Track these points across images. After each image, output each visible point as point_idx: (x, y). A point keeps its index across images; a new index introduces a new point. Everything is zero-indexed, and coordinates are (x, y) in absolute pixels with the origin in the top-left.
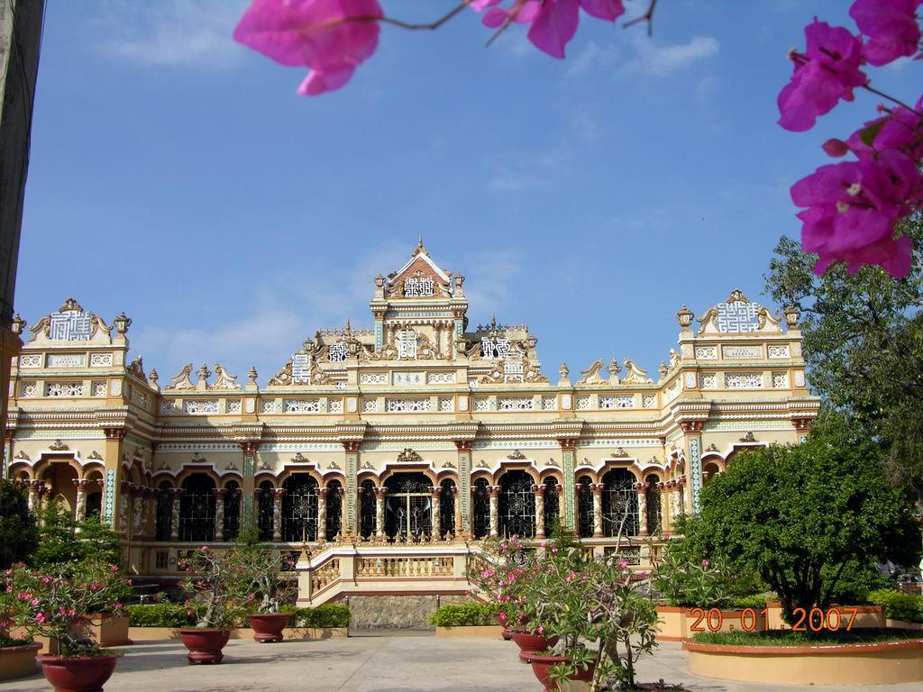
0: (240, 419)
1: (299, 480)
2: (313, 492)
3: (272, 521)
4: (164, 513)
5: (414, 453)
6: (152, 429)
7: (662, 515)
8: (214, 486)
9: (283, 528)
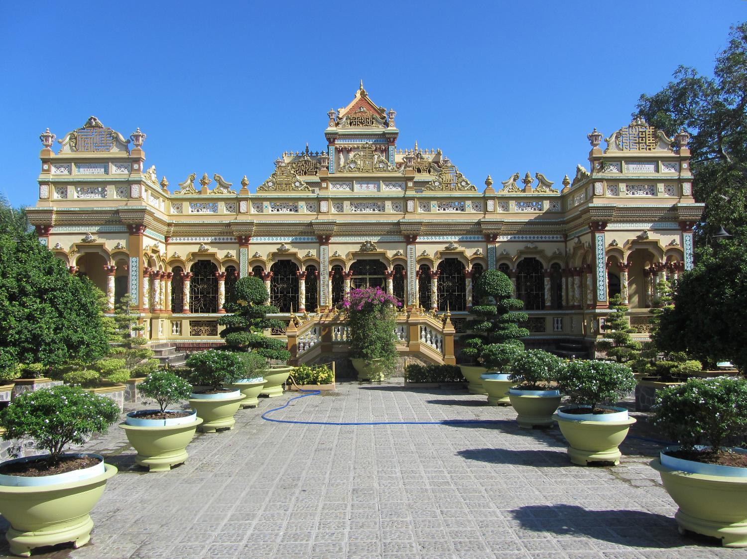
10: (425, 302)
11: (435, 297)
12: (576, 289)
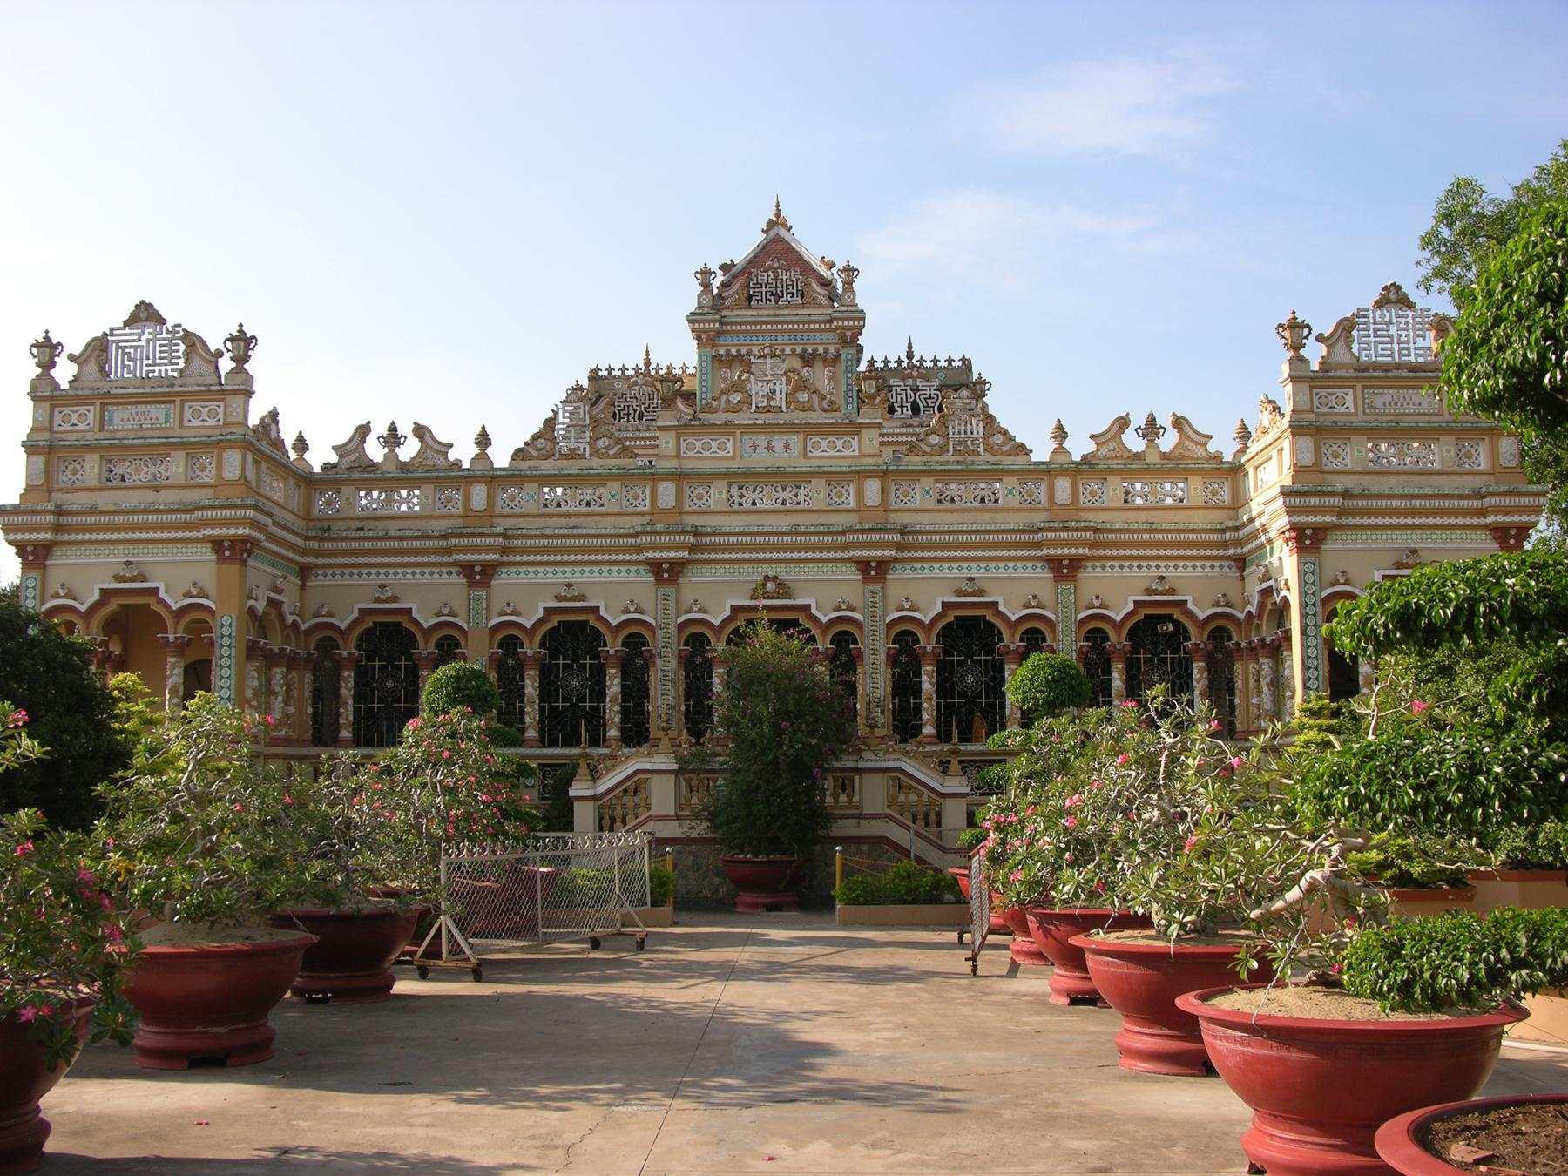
0: (459, 522)
1: (573, 636)
2: (596, 656)
3: (522, 708)
4: (324, 696)
5: (781, 584)
6: (300, 542)
7: (1237, 701)
8: (415, 644)
9: (541, 721)
10: (906, 727)
11: (928, 713)
12: (1265, 689)
